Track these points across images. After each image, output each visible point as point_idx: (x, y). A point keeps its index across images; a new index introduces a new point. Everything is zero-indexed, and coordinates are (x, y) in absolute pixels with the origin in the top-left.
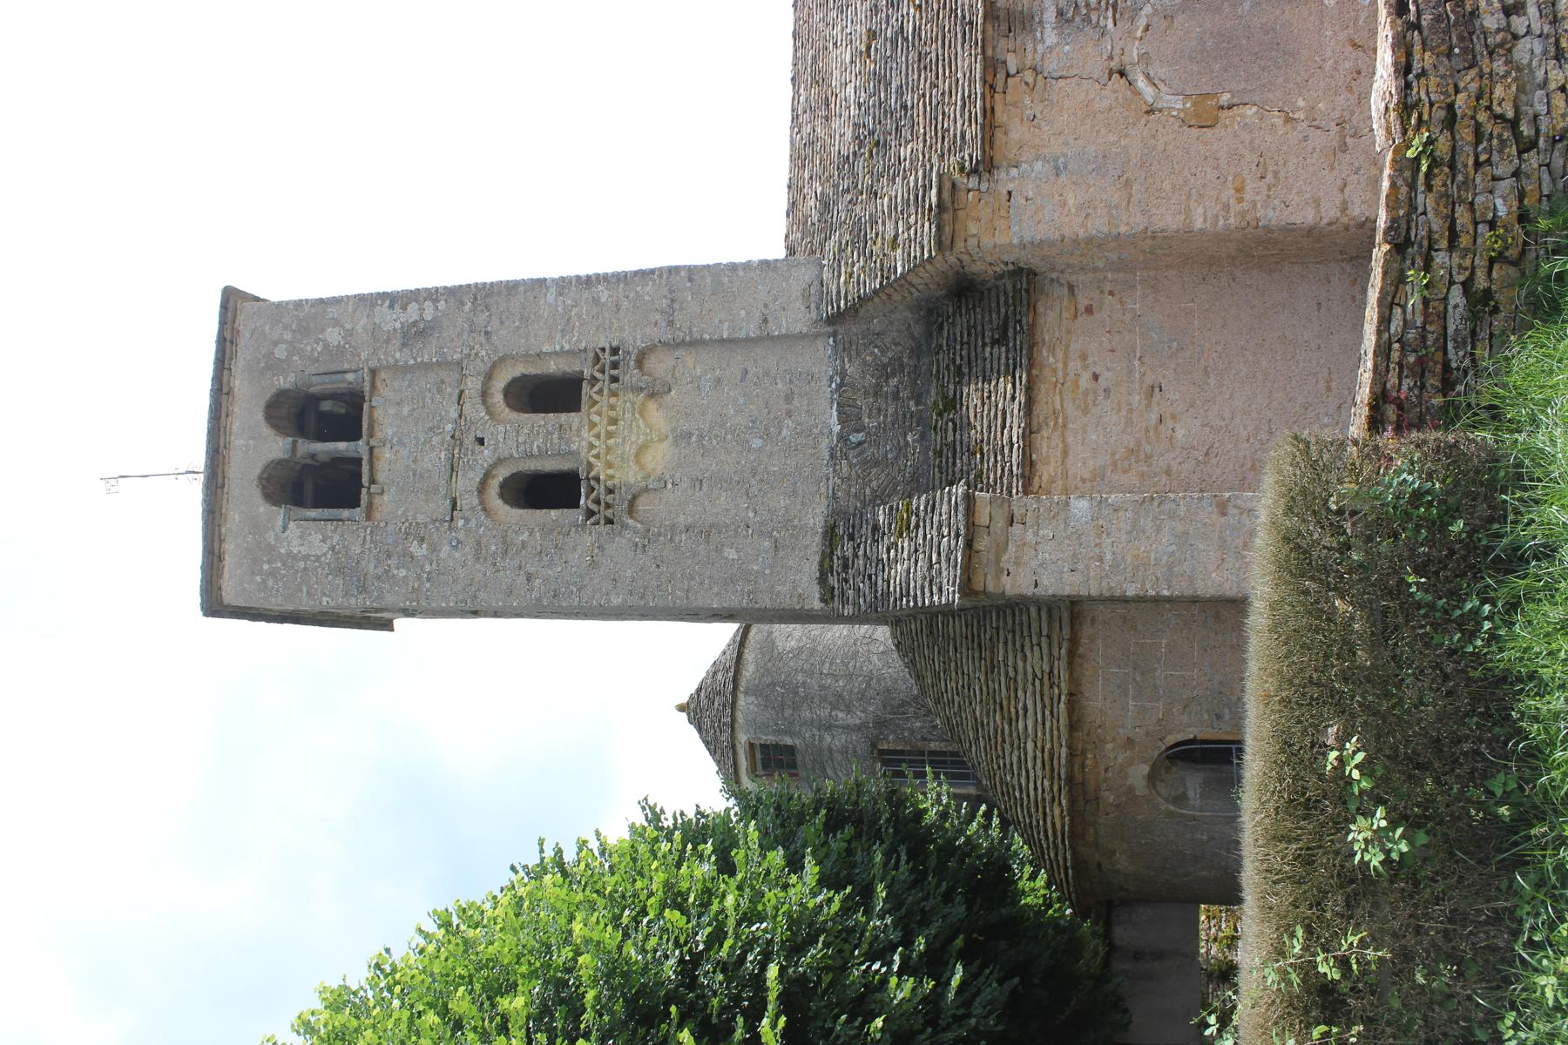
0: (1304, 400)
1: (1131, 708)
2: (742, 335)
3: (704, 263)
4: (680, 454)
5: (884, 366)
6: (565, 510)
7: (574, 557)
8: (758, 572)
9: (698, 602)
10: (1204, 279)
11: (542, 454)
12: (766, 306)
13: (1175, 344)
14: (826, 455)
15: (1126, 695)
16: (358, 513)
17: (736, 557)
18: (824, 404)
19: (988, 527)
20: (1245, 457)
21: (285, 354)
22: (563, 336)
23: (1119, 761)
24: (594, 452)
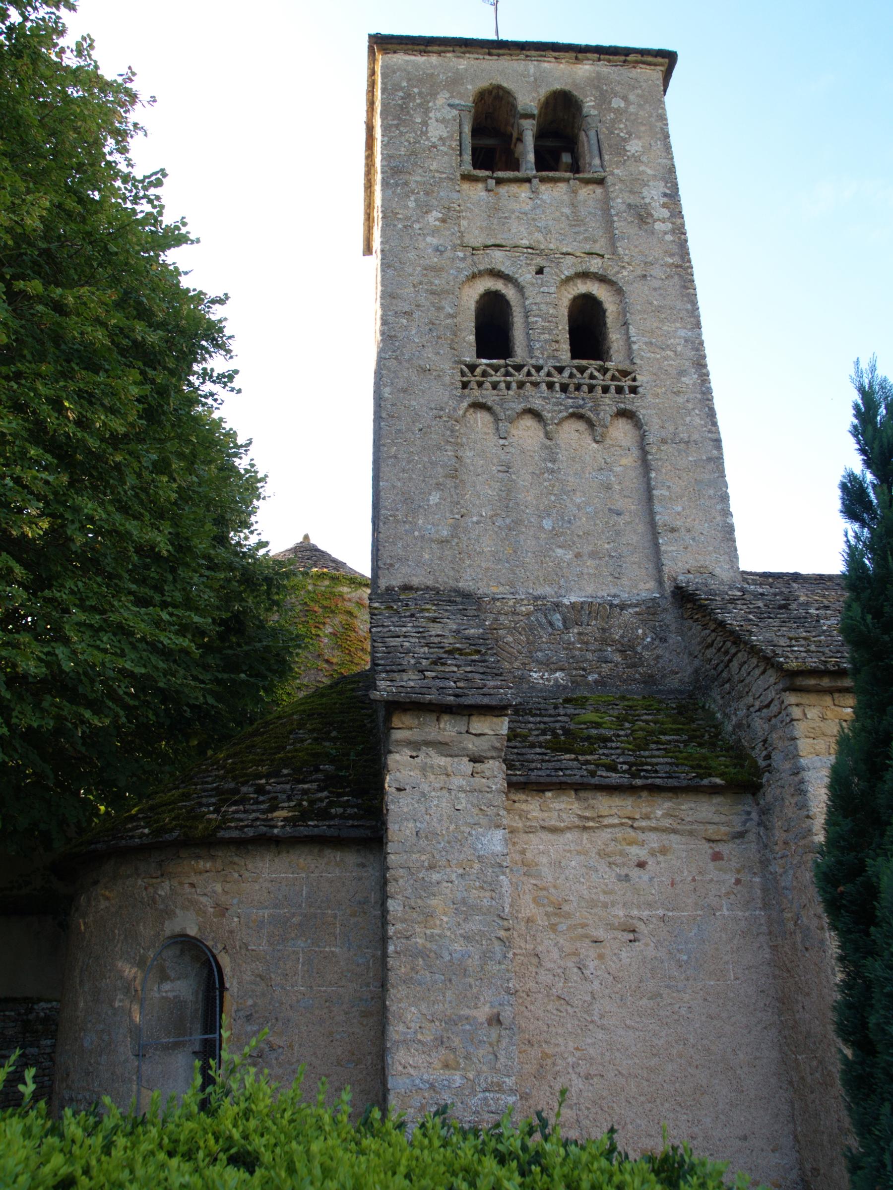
0: (628, 1120)
1: (261, 912)
2: (657, 508)
3: (727, 472)
4: (534, 452)
5: (633, 648)
6: (475, 349)
7: (429, 353)
8: (416, 524)
9: (384, 469)
10: (762, 991)
11: (528, 326)
12: (689, 531)
13: (685, 958)
14: (539, 592)
15: (276, 906)
16: (468, 167)
17: (431, 503)
18: (590, 590)
19: (467, 732)
20: (557, 1045)
21: (616, 106)
22: (646, 343)
23: (203, 899)
24: (533, 371)
